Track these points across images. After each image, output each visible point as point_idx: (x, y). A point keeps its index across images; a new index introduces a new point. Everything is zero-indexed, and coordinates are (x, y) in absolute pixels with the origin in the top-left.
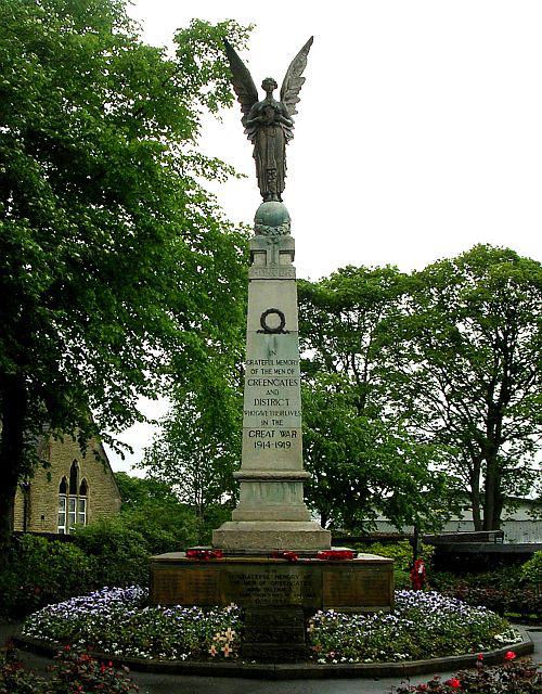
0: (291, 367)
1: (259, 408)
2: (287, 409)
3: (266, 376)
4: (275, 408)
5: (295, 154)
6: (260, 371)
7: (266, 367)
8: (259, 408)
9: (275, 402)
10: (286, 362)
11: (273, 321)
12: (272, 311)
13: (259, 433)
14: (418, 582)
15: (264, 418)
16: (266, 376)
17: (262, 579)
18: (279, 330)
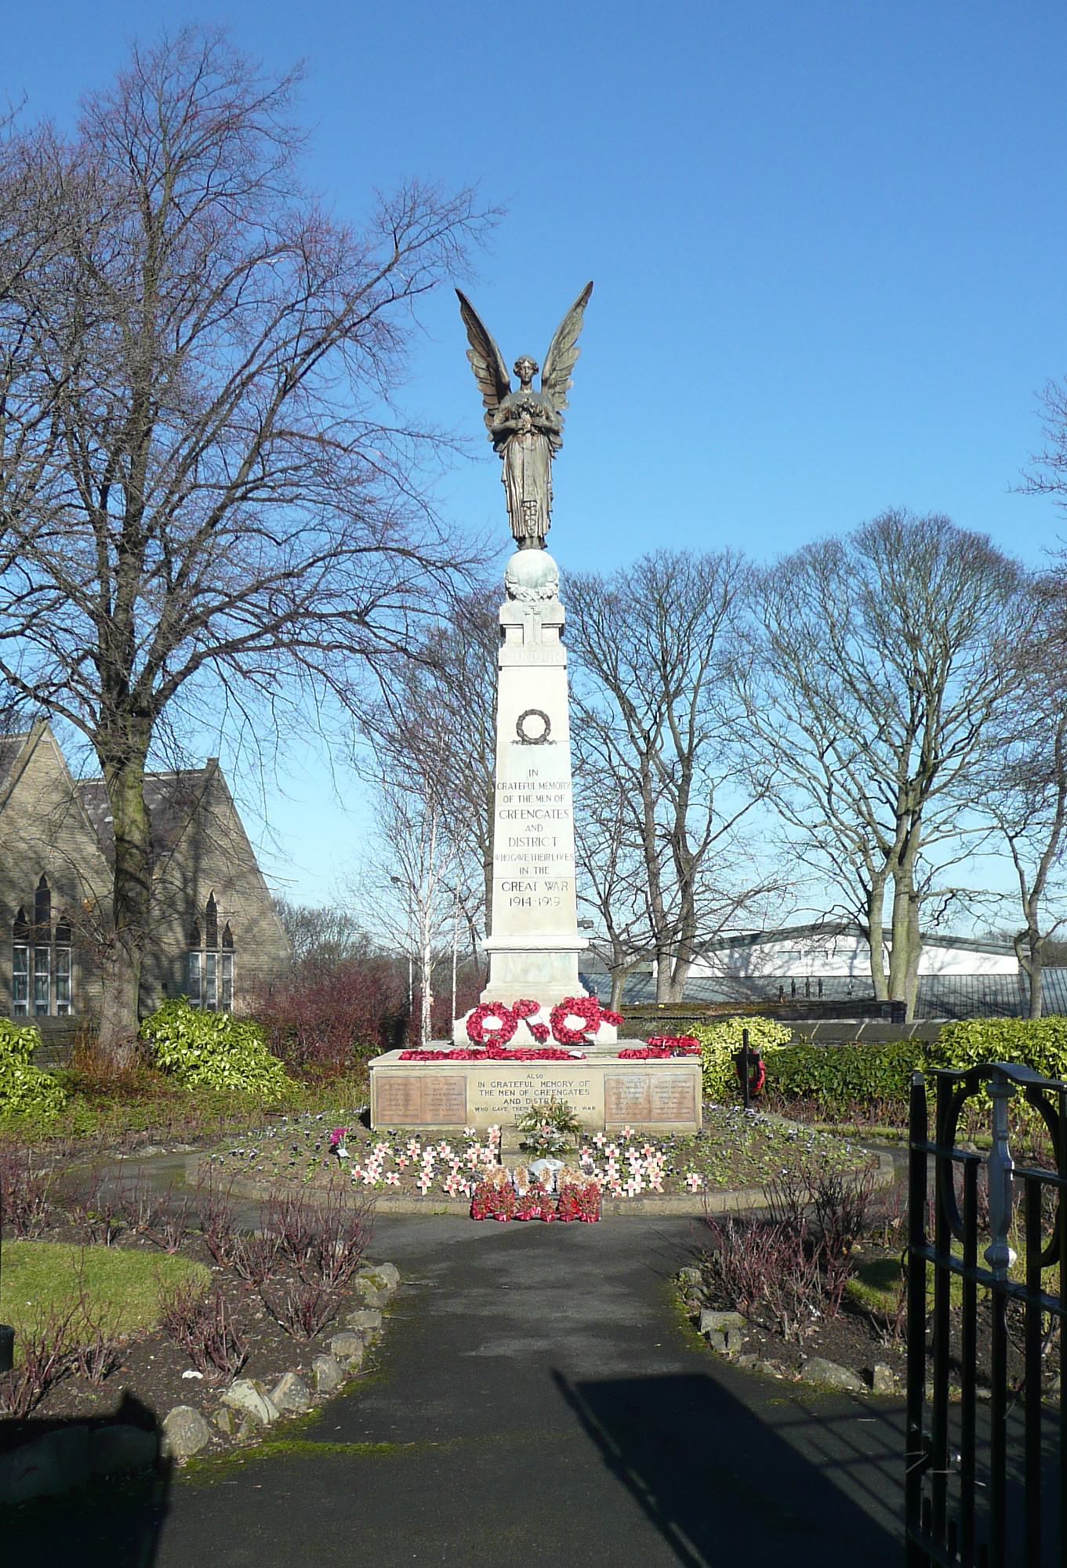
0: (560, 792)
1: (517, 850)
2: (554, 851)
3: (525, 806)
4: (535, 850)
5: (463, 329)
6: (515, 799)
7: (526, 792)
8: (517, 850)
9: (532, 842)
10: (553, 785)
11: (534, 728)
12: (548, 723)
13: (516, 886)
14: (925, 586)
15: (522, 864)
16: (525, 806)
17: (523, 1088)
18: (543, 739)
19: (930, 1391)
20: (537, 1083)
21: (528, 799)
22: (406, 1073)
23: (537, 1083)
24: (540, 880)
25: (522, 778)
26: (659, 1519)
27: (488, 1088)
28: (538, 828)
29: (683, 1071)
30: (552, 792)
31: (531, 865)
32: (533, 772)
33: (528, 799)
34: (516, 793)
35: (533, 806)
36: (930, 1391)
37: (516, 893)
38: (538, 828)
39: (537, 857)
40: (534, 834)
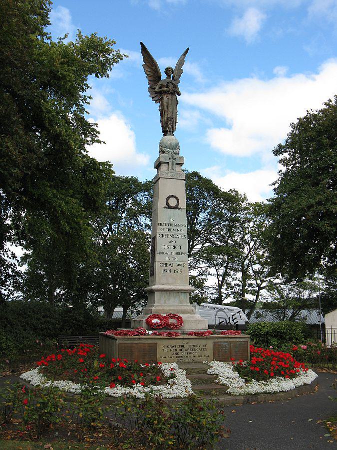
0: (182, 228)
3: (168, 232)
4: (173, 250)
7: (169, 227)
11: (172, 202)
15: (167, 256)
18: (176, 208)
19: (191, 243)
20: (186, 346)
21: (170, 230)
22: (132, 342)
23: (186, 346)
24: (175, 262)
25: (167, 222)
26: (268, 76)
27: (166, 348)
28: (174, 242)
29: (243, 340)
30: (179, 228)
31: (171, 256)
32: (172, 220)
33: (170, 230)
34: (165, 227)
35: (173, 233)
36: (191, 243)
37: (165, 268)
38: (174, 242)
39: (174, 253)
40: (172, 244)
